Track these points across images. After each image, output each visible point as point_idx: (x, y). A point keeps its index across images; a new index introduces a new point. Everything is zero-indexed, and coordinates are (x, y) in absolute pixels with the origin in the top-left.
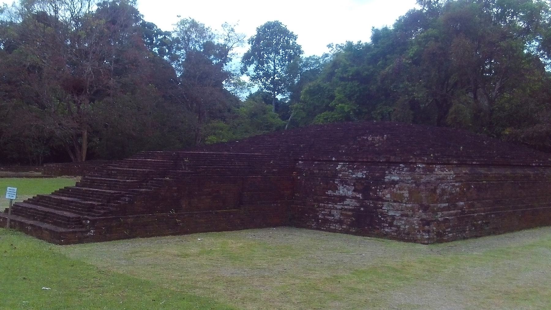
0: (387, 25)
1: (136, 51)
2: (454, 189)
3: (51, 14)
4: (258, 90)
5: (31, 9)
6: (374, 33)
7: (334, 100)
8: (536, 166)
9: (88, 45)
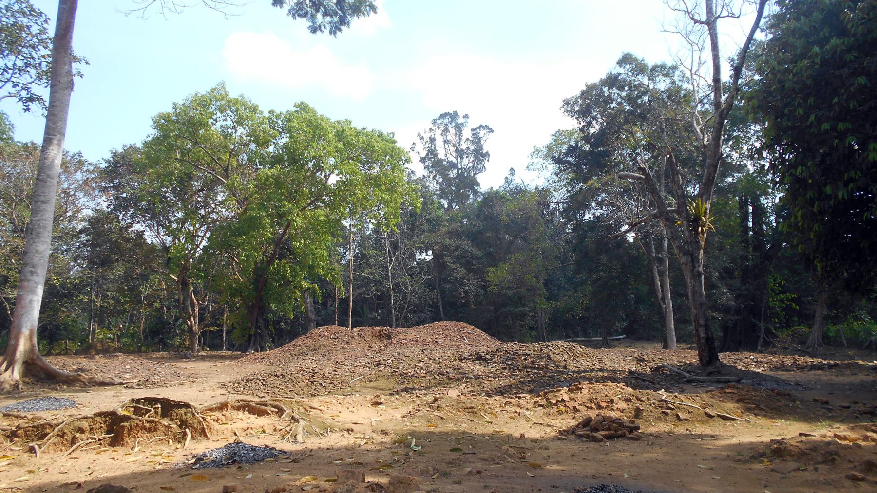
0: (537, 151)
1: (830, 193)
2: (80, 245)
3: (795, 467)
4: (82, 155)
5: (700, 229)
6: (106, 429)
7: (746, 166)
8: (605, 437)
9: (635, 239)
